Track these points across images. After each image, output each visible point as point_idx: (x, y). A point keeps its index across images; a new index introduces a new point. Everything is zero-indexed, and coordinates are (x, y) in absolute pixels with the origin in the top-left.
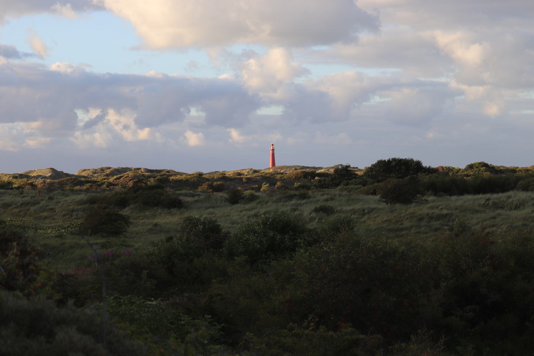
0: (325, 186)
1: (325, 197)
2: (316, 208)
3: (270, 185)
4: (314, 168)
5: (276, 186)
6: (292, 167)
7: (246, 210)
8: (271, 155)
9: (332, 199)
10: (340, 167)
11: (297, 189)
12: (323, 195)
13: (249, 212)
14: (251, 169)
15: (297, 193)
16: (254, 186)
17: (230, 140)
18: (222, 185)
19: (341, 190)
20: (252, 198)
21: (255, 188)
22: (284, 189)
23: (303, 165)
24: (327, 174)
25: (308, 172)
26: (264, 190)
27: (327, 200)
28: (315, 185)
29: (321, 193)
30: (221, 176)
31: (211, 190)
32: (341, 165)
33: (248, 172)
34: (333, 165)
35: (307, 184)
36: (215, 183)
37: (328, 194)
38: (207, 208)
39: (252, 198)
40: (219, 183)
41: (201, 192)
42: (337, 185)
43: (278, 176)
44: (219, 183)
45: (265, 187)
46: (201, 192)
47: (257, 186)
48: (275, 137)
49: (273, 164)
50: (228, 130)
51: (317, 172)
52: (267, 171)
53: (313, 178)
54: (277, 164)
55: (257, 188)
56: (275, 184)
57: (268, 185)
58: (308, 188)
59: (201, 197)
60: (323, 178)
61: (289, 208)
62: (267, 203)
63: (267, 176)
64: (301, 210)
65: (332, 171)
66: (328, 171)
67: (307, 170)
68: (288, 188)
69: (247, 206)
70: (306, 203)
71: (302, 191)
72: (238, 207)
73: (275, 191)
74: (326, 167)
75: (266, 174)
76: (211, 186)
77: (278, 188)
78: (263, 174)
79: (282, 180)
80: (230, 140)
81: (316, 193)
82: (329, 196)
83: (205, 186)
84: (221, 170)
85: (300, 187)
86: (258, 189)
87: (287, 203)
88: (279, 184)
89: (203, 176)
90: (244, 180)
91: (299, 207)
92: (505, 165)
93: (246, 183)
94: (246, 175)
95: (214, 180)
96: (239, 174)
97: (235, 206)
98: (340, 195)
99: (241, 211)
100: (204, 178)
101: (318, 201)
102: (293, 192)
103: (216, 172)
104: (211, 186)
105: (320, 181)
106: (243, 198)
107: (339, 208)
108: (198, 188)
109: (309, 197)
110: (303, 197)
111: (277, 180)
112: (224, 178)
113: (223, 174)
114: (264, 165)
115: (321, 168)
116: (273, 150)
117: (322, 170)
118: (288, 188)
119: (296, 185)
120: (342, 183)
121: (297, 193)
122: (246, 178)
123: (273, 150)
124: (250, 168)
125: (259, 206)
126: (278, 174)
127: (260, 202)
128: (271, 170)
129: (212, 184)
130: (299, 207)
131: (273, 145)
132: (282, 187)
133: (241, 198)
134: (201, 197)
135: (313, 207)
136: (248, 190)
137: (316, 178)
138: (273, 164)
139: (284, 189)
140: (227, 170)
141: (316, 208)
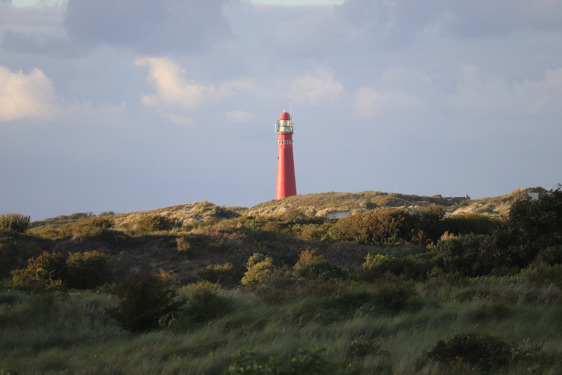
0: (475, 266)
1: (476, 304)
2: (441, 344)
3: (277, 263)
4: (439, 200)
5: (297, 266)
6: (357, 197)
7: (184, 352)
8: (280, 153)
9: (501, 313)
10: (535, 197)
11: (373, 275)
12: (468, 296)
13: (196, 361)
14: (208, 207)
15: (372, 289)
16: (218, 267)
17: (147, 100)
18: (98, 263)
19: (538, 280)
20: (207, 310)
21: (219, 272)
22: (326, 279)
23: (397, 191)
24: (485, 221)
25: (416, 217)
26: (256, 282)
27: (480, 316)
28: (440, 263)
29: (462, 290)
30: (96, 230)
31: (59, 282)
32: (539, 190)
33: (197, 216)
34: (508, 191)
35: (411, 257)
36: (73, 258)
37: (484, 294)
38: (39, 347)
39: (207, 310)
40: (87, 255)
41: (21, 289)
42: (521, 263)
43: (307, 231)
44: (87, 255)
45: (256, 269)
46: (21, 289)
47: (226, 266)
48: (311, 91)
49: (289, 187)
50: (140, 62)
51: (447, 215)
52: (265, 214)
53: (435, 235)
54: (303, 188)
55: (227, 272)
56: (292, 260)
57: (267, 262)
58: (419, 273)
59: (19, 308)
60: (468, 238)
61: (341, 343)
62: (261, 325)
63: (266, 228)
64: (387, 354)
65: (504, 210)
66: (490, 210)
67: (414, 208)
68: (340, 274)
69: (190, 340)
70: (406, 326)
71: (392, 283)
72: (158, 340)
73: (290, 283)
74: (481, 196)
75: (263, 222)
76: (58, 269)
77: (304, 273)
78: (250, 224)
79: (321, 245)
80: (147, 100)
81: (442, 291)
82: (489, 303)
83: (36, 267)
84: (97, 210)
85: (383, 268)
86: (233, 278)
87: (334, 327)
88: (306, 258)
89: (33, 231)
90: (182, 246)
91: (376, 343)
92: (313, 192)
93: (190, 254)
94: (190, 228)
95: (68, 245)
96: (164, 223)
97: (143, 338)
98: (530, 299)
99: (165, 358)
100: (32, 238)
101: (448, 319)
102: (354, 288)
103: (77, 216)
104: (58, 269)
105: (457, 248)
106: (175, 308)
107: (526, 345)
108: (10, 277)
109: (417, 306)
110: (394, 303)
111: (302, 245)
112: (106, 235)
113: (105, 223)
114: (256, 193)
115: (464, 201)
116: (288, 136)
117: (468, 210)
118: (340, 274)
119: (371, 261)
120: (539, 256)
121: (372, 289)
122: (188, 239)
123: (288, 136)
124: (203, 200)
125: (231, 335)
126: (304, 221)
127: (235, 325)
128: (281, 210)
129: (63, 260)
130: (376, 343)
131: (286, 117)
132: (318, 269)
133: (168, 310)
134: (19, 308)
135: (429, 340)
136: (195, 281)
137: (445, 237)
138: (289, 187)
139: (326, 279)
140: (117, 211)
141: (441, 344)
